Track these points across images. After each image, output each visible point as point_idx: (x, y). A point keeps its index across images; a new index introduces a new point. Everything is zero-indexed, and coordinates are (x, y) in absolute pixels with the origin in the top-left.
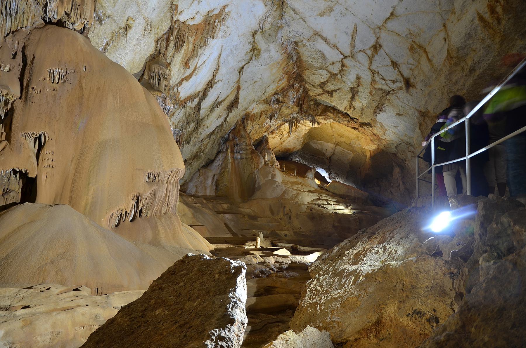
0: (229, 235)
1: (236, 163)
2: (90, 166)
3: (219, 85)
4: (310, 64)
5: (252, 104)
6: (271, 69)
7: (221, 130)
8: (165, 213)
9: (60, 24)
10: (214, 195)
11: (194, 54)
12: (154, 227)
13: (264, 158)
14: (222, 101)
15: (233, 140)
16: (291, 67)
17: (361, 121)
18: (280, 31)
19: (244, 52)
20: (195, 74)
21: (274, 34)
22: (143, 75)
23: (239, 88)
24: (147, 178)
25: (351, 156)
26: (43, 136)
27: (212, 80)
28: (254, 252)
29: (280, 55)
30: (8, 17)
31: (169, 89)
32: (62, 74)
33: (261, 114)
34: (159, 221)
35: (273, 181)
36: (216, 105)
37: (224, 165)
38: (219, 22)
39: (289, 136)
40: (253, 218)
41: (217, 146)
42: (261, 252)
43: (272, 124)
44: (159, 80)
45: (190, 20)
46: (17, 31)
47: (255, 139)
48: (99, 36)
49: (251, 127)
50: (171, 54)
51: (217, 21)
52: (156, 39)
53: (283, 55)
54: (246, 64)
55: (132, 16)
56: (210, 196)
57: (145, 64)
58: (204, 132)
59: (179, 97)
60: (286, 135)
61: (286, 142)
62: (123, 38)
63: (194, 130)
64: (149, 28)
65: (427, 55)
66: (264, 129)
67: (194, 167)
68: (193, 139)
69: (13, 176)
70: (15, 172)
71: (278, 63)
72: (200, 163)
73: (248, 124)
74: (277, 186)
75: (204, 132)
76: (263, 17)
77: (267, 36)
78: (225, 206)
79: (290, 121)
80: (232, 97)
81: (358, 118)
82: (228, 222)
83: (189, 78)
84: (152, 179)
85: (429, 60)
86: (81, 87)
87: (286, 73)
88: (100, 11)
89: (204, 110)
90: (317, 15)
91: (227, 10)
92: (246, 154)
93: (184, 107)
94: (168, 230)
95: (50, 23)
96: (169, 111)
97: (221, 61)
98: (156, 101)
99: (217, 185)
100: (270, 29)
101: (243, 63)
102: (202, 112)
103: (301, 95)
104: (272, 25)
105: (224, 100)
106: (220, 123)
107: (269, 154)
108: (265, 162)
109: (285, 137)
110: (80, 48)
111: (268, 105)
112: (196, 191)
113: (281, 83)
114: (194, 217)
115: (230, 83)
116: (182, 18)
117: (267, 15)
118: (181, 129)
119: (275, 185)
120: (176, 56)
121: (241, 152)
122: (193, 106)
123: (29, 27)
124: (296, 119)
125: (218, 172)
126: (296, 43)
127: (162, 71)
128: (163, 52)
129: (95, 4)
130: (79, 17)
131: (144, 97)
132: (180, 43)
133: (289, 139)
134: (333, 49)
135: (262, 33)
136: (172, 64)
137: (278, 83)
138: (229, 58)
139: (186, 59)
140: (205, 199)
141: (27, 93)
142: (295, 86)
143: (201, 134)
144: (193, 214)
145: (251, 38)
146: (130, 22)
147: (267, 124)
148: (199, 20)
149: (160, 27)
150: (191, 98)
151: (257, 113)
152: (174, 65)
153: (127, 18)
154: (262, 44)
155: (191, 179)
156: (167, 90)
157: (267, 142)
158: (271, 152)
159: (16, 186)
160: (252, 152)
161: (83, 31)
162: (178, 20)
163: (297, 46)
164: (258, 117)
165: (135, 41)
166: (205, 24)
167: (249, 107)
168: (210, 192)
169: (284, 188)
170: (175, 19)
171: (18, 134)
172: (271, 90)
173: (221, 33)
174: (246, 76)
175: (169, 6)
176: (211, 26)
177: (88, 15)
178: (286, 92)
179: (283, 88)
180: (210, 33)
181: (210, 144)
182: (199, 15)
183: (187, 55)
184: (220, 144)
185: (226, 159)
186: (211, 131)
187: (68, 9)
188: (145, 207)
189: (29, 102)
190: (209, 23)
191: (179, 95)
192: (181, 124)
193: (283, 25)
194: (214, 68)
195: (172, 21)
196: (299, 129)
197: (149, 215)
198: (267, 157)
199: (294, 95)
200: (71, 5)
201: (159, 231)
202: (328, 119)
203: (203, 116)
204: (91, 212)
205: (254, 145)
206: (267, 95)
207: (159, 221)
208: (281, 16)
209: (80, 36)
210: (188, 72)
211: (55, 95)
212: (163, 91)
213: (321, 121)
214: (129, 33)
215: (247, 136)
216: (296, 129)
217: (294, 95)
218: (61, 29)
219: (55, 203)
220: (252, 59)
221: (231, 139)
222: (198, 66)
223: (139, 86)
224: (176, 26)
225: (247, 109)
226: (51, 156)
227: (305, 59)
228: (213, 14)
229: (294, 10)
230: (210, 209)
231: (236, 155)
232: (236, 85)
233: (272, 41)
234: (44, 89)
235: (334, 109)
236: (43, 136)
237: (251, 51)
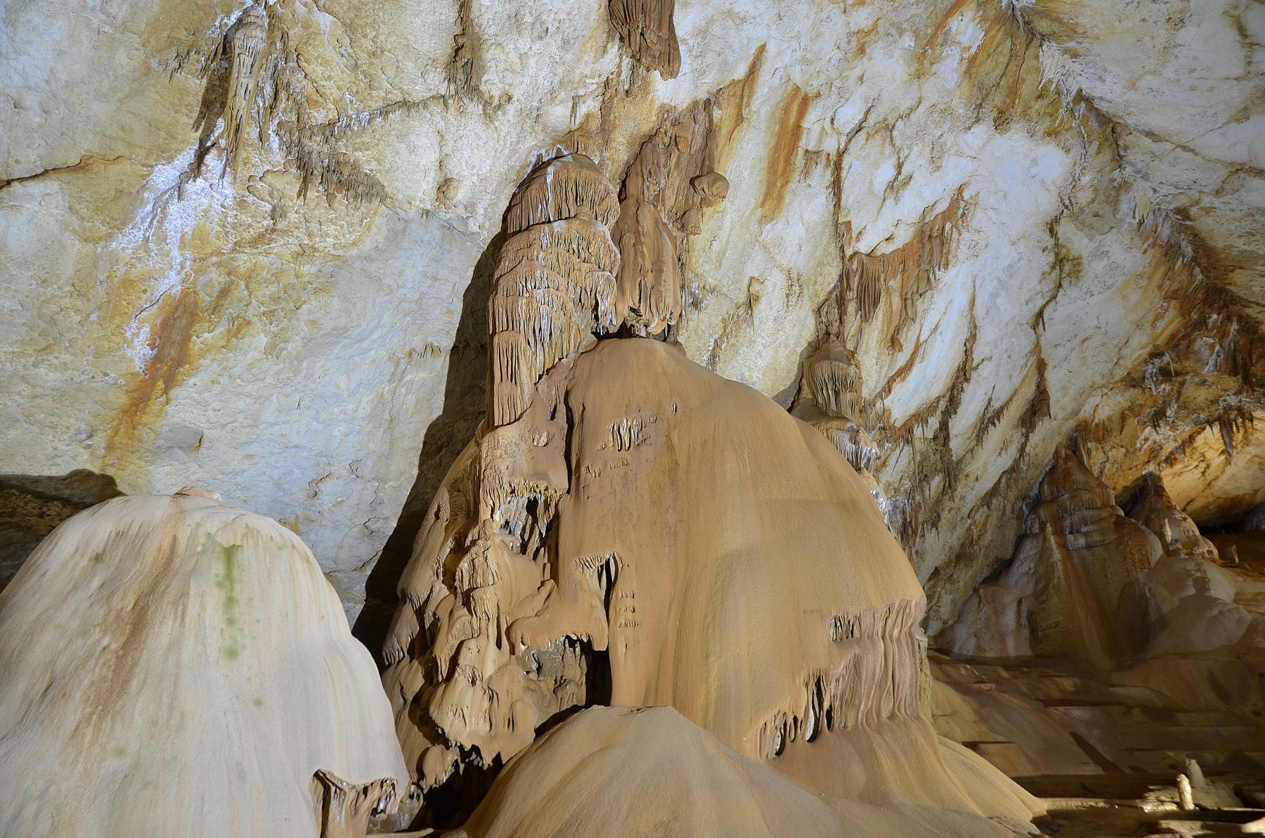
0: (1091, 770)
1: (1076, 561)
2: (706, 616)
3: (986, 370)
4: (1243, 252)
5: (1089, 396)
6: (1124, 297)
7: (1016, 481)
8: (892, 717)
9: (625, 332)
10: (1029, 653)
11: (907, 314)
12: (868, 755)
13: (1161, 536)
14: (1002, 408)
15: (1055, 499)
16: (1184, 277)
18: (1123, 197)
20: (918, 359)
21: (1108, 208)
22: (800, 389)
23: (1041, 367)
24: (832, 630)
26: (612, 560)
27: (965, 363)
28: (1173, 825)
29: (1138, 254)
30: (539, 346)
31: (864, 409)
32: (635, 430)
33: (1123, 418)
34: (878, 737)
35: (1203, 599)
36: (989, 419)
37: (1041, 570)
38: (955, 226)
39: (1228, 462)
40: (1162, 713)
41: (1014, 522)
42: (1198, 824)
43: (1166, 437)
44: (837, 394)
45: (884, 244)
46: (553, 367)
47: (1119, 488)
48: (698, 335)
49: (1101, 456)
50: (853, 331)
51: (948, 226)
52: (815, 306)
53: (1150, 252)
55: (756, 275)
56: (1018, 657)
57: (801, 366)
58: (971, 491)
59: (892, 421)
60: (1217, 460)
61: (1223, 478)
62: (745, 325)
63: (943, 493)
64: (796, 288)
66: (1142, 456)
67: (961, 584)
68: (945, 515)
69: (569, 650)
70: (572, 643)
71: (1141, 276)
72: (974, 574)
73: (1089, 452)
74: (1221, 613)
75: (971, 491)
77: (1090, 219)
78: (1067, 684)
79: (1219, 419)
80: (1029, 392)
82: (1082, 731)
83: (904, 375)
84: (846, 632)
86: (671, 447)
87: (1171, 296)
88: (695, 285)
89: (959, 439)
90: (1228, 122)
92: (1102, 532)
93: (907, 442)
94: (903, 760)
95: (608, 336)
96: (869, 460)
97: (979, 311)
98: (832, 445)
99: (1033, 624)
100: (1093, 201)
101: (1040, 302)
102: (954, 444)
103: (1236, 343)
104: (1096, 190)
105: (1007, 404)
106: (1010, 463)
107: (1174, 522)
108: (1165, 546)
109: (1213, 467)
110: (660, 370)
111: (1137, 391)
112: (978, 647)
113: (1161, 325)
114: (982, 719)
115: (1014, 358)
116: (864, 247)
117: (1078, 171)
118: (910, 494)
119: (1215, 612)
120: (867, 329)
121: (1084, 529)
122: (930, 435)
123: (572, 355)
124: (1239, 409)
125: (1030, 591)
126: (1183, 212)
127: (839, 373)
128: (834, 329)
129: (683, 275)
130: (654, 310)
131: (802, 441)
132: (869, 301)
133: (1230, 470)
135: (1074, 217)
136: (861, 352)
137: (1153, 325)
138: (999, 301)
139: (892, 330)
140: (1006, 668)
141: (578, 479)
142: (1210, 322)
143: (963, 498)
144: (977, 712)
145: (1047, 236)
146: (756, 288)
147: (1146, 440)
148: (904, 236)
149: (820, 279)
150: (920, 417)
151: (1110, 418)
152: (866, 352)
153: (747, 282)
154: (1076, 240)
155: (960, 616)
156: (857, 411)
157: (1159, 490)
158: (1178, 516)
159: (576, 670)
160: (1119, 524)
161: (667, 336)
162: (856, 253)
163: (1188, 218)
164: (1116, 427)
165: (770, 323)
166: (921, 241)
167: (1082, 405)
168: (1015, 647)
169: (1249, 617)
170: (849, 252)
171: (570, 566)
172: (1139, 345)
174: (1055, 328)
175: (830, 229)
177: (670, 301)
178: (1184, 344)
179: (1173, 336)
181: (993, 520)
182: (902, 226)
183: (890, 323)
184: (1020, 517)
185: (1044, 553)
186: (990, 485)
187: (632, 300)
188: (837, 703)
189: (583, 497)
190: (930, 237)
191: (889, 417)
192: (907, 484)
193: (1131, 180)
194: (965, 334)
195: (843, 258)
196: (1257, 435)
197: (850, 724)
198: (1169, 533)
199: (1212, 346)
200: (637, 292)
201: (879, 764)
203: (961, 453)
204: (717, 722)
205: (1122, 505)
206: (1128, 364)
207: (877, 739)
208: (1118, 160)
209: (659, 346)
210: (902, 359)
211: (626, 473)
212: (849, 416)
214: (756, 311)
215: (1093, 483)
216: (1245, 438)
217: (1212, 346)
218: (626, 342)
220: (1060, 286)
221: (1049, 498)
222: (922, 340)
223: (791, 422)
224: (854, 267)
225: (1076, 413)
226: (629, 602)
227: (1221, 245)
228: (934, 214)
229: (1151, 134)
230: (1022, 695)
231: (1070, 538)
232: (1033, 359)
233: (1107, 227)
234: (605, 466)
236: (612, 560)
237: (1053, 268)
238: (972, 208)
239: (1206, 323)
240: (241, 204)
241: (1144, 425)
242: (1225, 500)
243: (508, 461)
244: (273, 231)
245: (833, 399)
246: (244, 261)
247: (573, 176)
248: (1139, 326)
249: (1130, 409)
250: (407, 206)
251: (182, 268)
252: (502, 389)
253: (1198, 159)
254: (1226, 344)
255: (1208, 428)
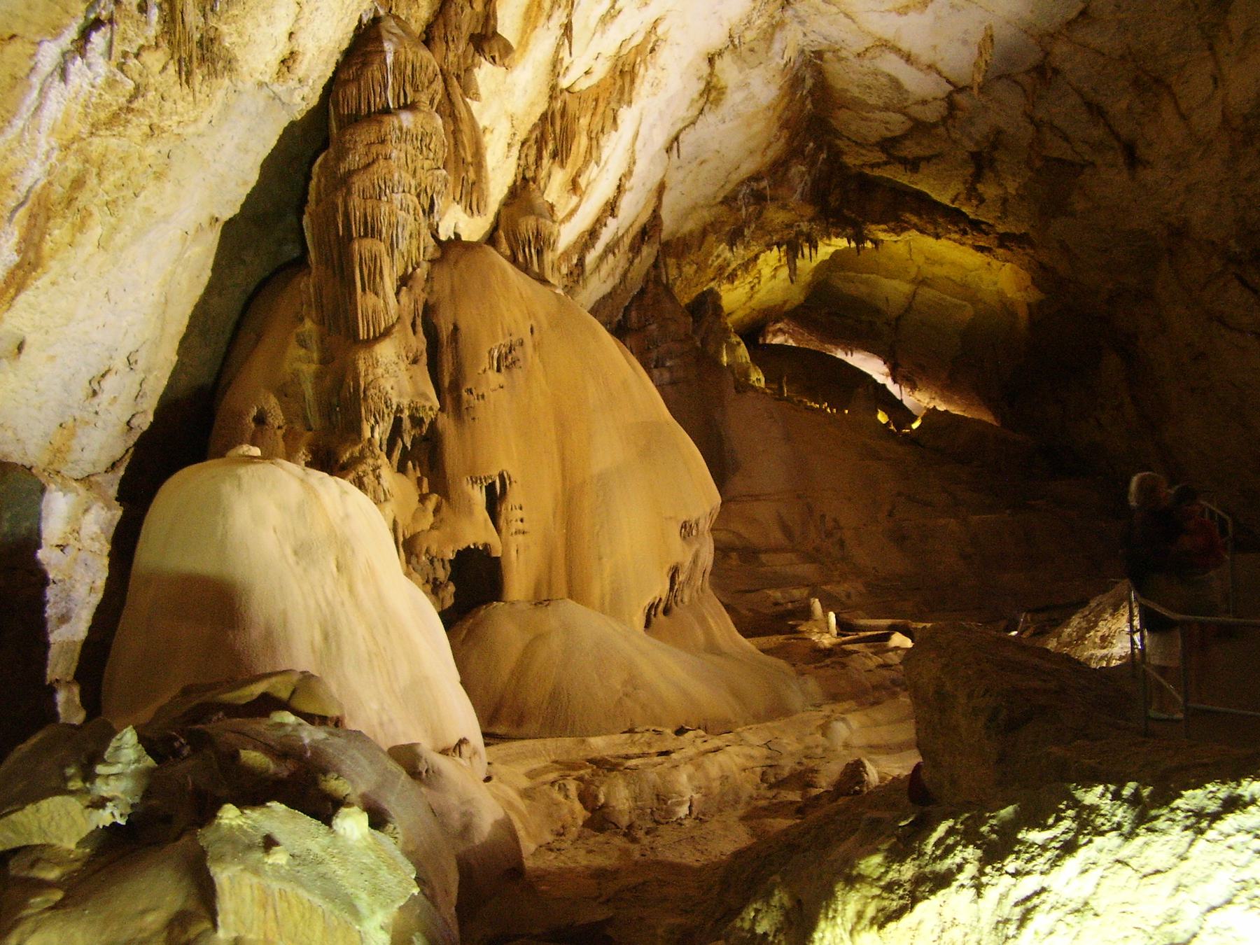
15: (642, 328)
17: (1001, 229)
18: (778, 36)
19: (687, 102)
25: (969, 312)
36: (610, 249)
54: (684, 128)
65: (1176, 102)
66: (710, 273)
76: (741, 20)
81: (991, 222)
85: (1183, 117)
91: (660, 30)
101: (680, 125)
106: (609, 290)
130: (475, 207)
134: (927, 75)
142: (807, 150)
147: (718, 256)
148: (601, 70)
151: (691, 233)
154: (728, 71)
157: (718, 309)
173: (647, 86)
176: (628, 79)
180: (626, 96)
190: (621, 71)
202: (904, 230)
204: (613, 608)
213: (882, 236)
217: (803, 174)
219: (541, 600)
235: (921, 197)
237: (701, 95)
238: (663, 44)
239: (802, 152)
240: (111, 84)
241: (720, 241)
242: (759, 312)
243: (392, 381)
244: (130, 110)
245: (535, 258)
246: (97, 145)
247: (410, 56)
248: (751, 153)
249: (712, 224)
250: (248, 78)
251: (48, 157)
252: (366, 302)
253: (854, 27)
254: (813, 172)
255: (775, 248)
